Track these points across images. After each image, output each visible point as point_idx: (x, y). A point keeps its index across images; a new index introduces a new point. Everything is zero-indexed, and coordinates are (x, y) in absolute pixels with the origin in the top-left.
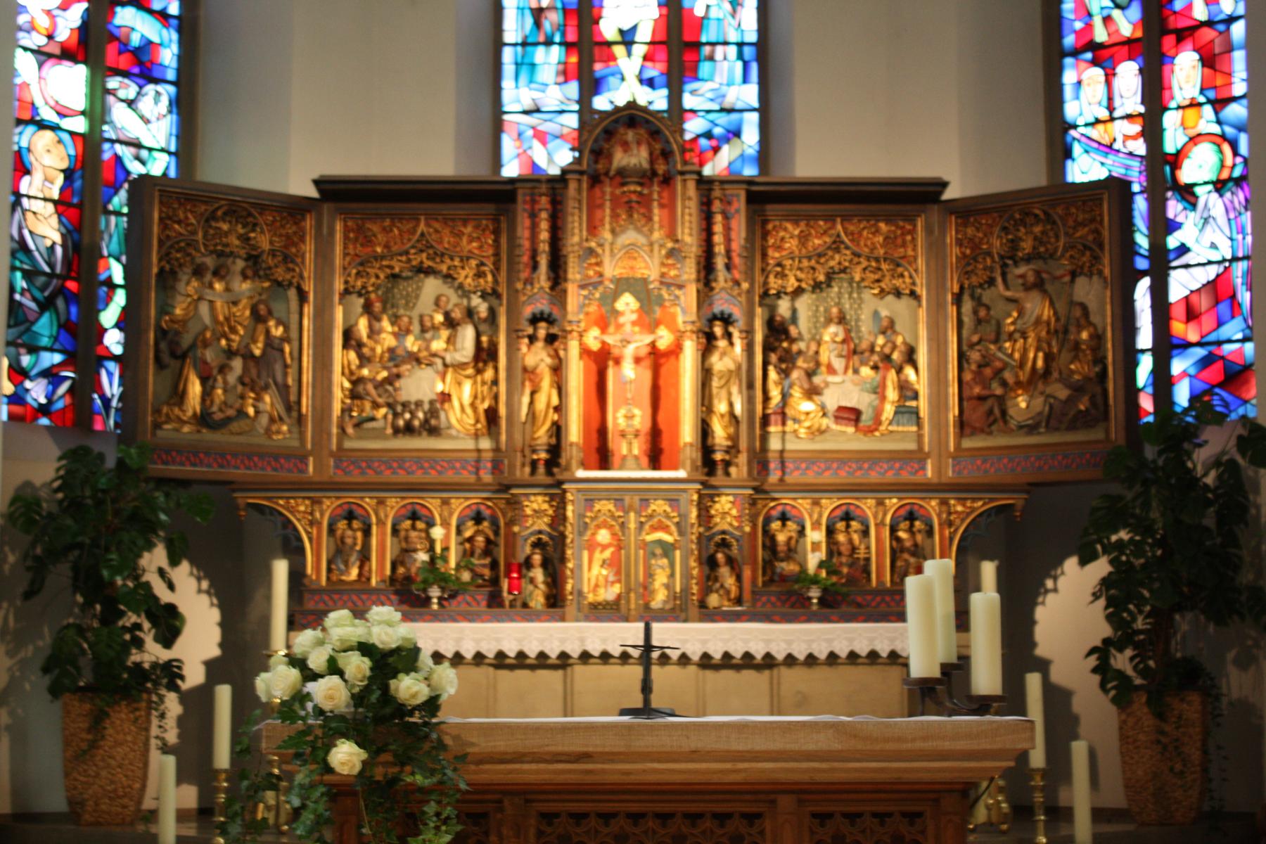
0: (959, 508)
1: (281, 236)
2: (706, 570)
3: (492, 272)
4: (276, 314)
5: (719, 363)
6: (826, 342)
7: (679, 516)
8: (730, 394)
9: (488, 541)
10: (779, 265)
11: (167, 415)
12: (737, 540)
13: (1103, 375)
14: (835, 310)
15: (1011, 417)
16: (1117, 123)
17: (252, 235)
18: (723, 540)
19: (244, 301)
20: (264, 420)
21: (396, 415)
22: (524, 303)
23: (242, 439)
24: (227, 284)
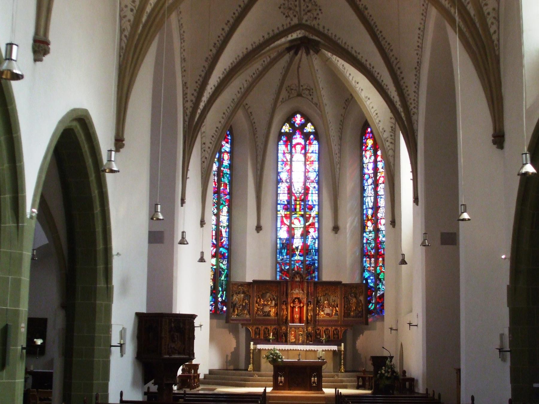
5: (309, 308)
9: (277, 332)
21: (263, 314)
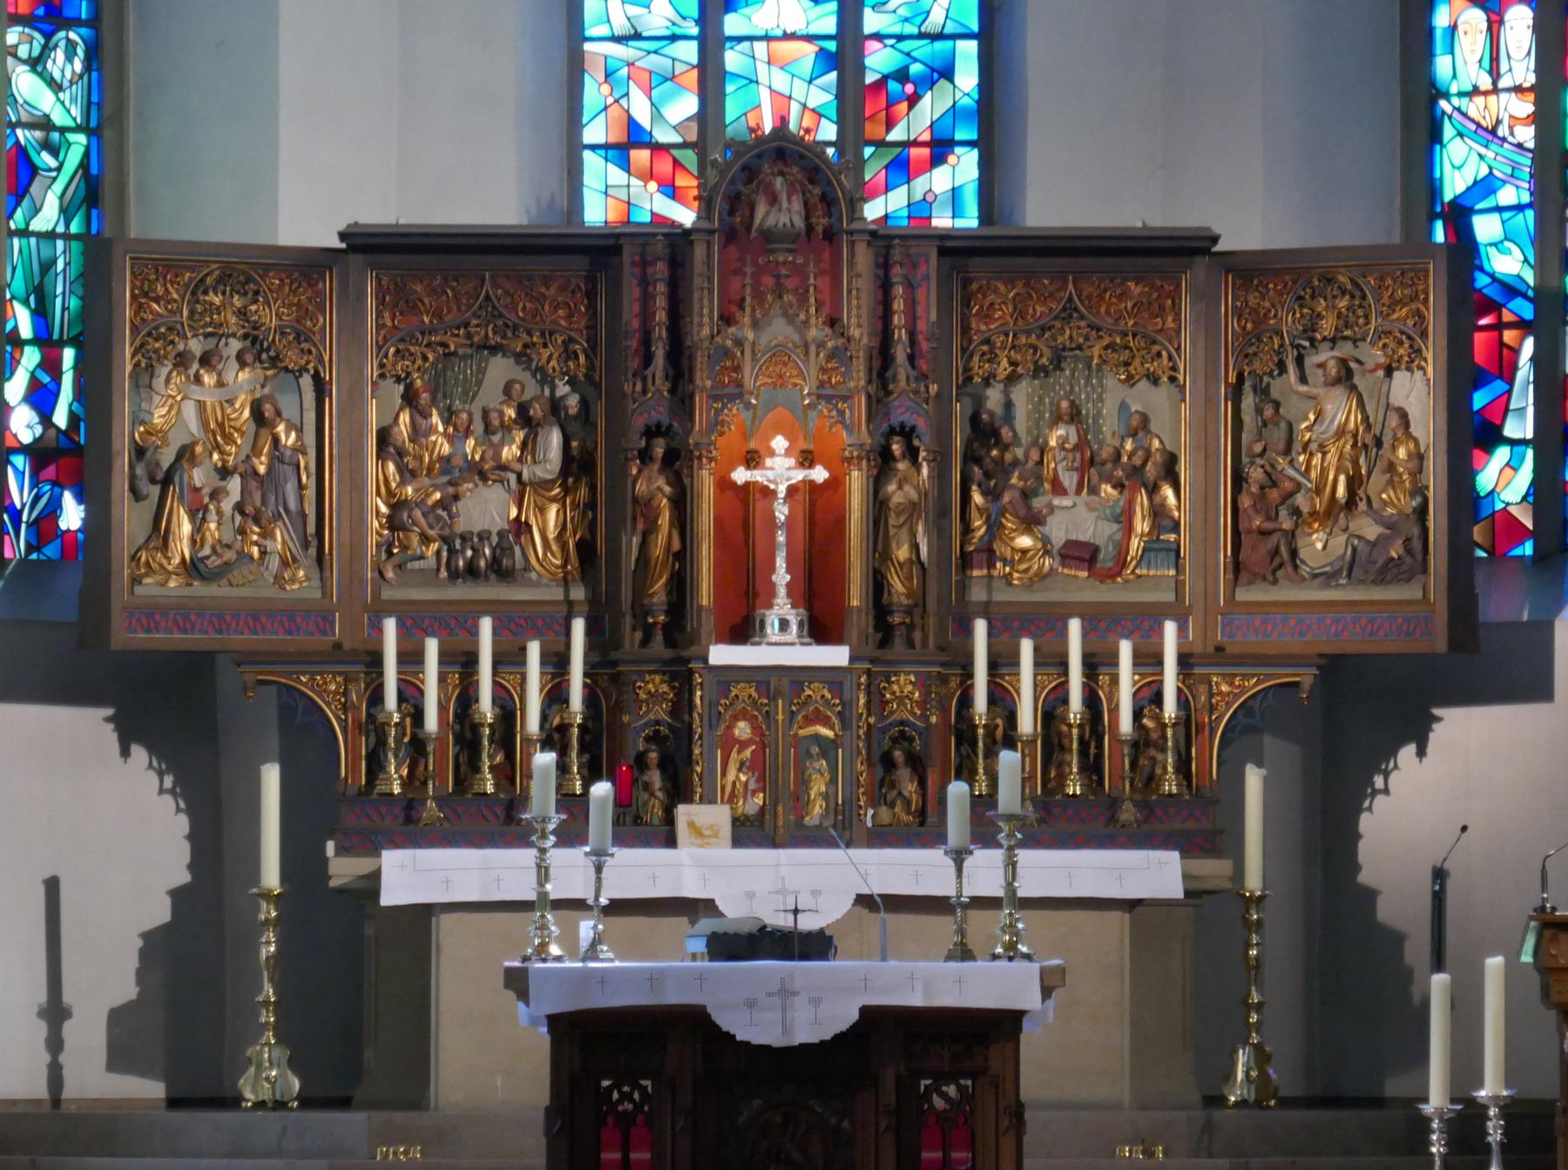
0: (1225, 688)
1: (291, 305)
2: (879, 771)
3: (584, 351)
4: (285, 414)
6: (1053, 449)
7: (843, 703)
8: (913, 535)
10: (987, 341)
11: (147, 563)
12: (920, 734)
13: (1422, 512)
14: (1065, 404)
15: (1303, 561)
16: (1504, 96)
17: (253, 308)
18: (902, 732)
19: (242, 398)
20: (274, 563)
21: (452, 552)
22: (634, 411)
23: (245, 592)
24: (219, 375)
